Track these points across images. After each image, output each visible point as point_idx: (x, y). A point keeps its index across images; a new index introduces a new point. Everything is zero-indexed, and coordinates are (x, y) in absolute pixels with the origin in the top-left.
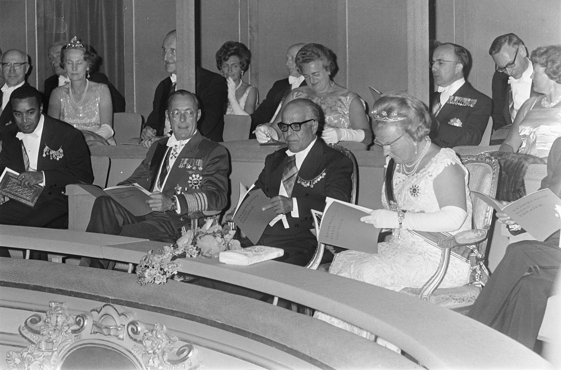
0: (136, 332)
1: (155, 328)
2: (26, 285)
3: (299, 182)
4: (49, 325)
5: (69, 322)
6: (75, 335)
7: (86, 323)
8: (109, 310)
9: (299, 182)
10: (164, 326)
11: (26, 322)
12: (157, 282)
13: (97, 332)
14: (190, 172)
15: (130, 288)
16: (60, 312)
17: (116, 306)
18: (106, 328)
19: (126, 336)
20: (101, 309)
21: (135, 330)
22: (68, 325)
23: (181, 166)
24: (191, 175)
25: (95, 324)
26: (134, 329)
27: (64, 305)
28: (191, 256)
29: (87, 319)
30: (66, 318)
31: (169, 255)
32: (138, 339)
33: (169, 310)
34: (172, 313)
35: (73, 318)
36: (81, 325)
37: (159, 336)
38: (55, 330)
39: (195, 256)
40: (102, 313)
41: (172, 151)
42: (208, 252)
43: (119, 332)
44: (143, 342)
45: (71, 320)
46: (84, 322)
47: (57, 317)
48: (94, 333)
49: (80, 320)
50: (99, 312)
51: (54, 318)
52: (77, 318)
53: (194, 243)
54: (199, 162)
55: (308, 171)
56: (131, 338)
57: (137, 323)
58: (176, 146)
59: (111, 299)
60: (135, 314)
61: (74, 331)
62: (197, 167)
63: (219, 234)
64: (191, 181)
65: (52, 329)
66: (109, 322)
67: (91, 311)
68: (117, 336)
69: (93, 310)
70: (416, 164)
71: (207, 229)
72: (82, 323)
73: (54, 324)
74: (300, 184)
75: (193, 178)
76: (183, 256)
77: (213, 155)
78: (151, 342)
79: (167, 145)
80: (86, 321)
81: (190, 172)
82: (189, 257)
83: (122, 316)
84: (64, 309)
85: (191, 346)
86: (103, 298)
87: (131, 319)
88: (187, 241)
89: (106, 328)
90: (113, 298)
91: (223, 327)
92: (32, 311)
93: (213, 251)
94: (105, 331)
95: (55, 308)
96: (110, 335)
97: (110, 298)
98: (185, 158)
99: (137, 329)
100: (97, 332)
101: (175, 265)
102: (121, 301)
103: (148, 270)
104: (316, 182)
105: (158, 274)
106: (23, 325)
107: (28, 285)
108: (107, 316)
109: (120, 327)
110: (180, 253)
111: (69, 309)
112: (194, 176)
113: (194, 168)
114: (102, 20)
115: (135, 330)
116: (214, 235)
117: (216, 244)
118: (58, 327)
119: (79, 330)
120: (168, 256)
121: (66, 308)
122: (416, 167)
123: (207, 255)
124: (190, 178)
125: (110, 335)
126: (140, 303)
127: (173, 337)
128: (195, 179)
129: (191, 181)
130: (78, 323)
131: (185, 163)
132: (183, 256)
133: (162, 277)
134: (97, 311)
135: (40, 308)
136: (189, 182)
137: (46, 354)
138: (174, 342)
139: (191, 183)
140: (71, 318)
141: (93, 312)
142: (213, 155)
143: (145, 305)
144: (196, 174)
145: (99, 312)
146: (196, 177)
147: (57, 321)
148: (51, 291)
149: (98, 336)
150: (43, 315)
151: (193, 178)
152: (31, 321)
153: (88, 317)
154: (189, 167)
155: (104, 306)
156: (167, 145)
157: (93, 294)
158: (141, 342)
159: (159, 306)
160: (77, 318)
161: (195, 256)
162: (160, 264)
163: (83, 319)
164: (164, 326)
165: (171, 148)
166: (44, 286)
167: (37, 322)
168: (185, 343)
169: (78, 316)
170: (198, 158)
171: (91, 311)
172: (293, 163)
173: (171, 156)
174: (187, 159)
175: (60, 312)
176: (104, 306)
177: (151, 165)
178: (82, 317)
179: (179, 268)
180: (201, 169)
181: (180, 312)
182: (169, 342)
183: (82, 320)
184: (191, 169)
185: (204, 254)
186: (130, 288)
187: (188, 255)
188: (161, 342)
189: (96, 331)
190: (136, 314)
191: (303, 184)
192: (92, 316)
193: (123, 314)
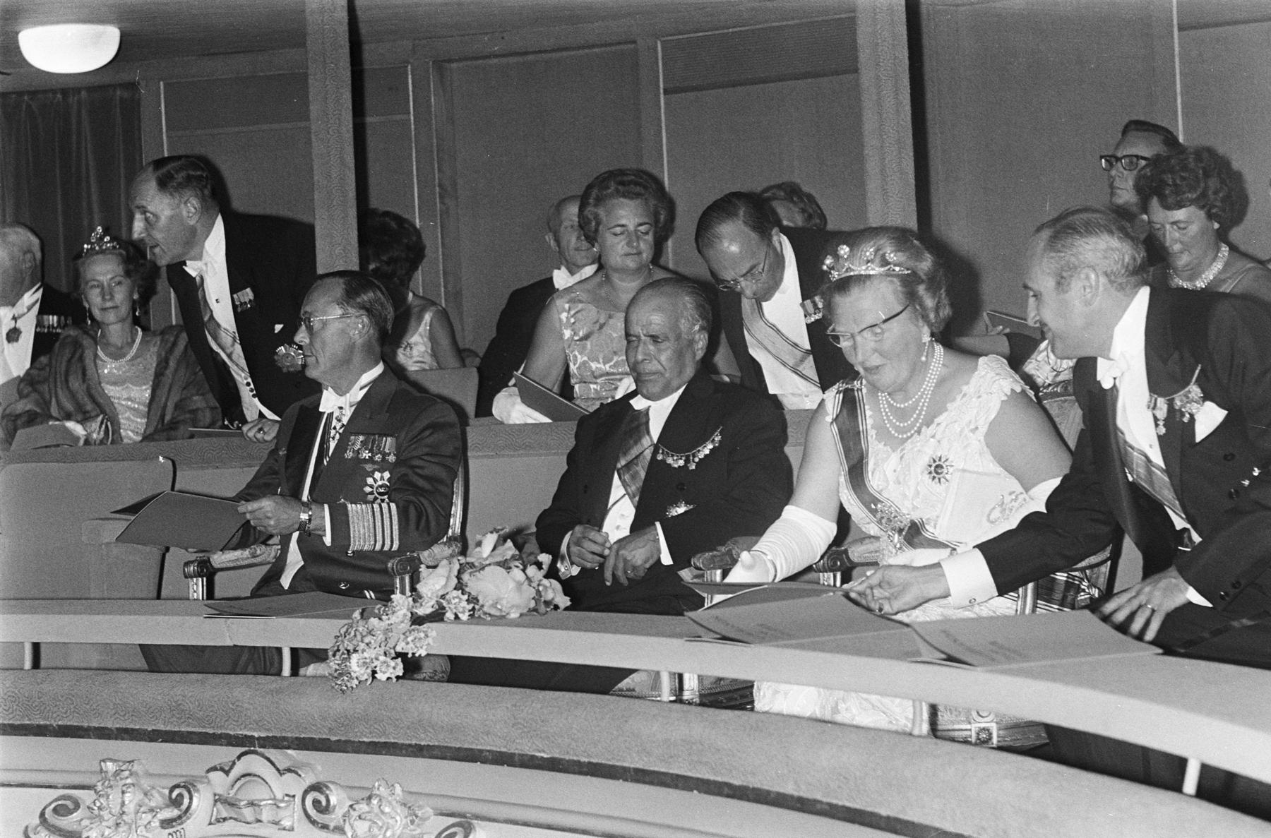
0: (323, 809)
1: (376, 792)
2: (39, 726)
3: (660, 457)
4: (105, 814)
5: (153, 804)
6: (171, 830)
7: (195, 800)
8: (254, 763)
9: (660, 457)
10: (397, 786)
11: (42, 815)
12: (381, 676)
13: (225, 819)
14: (369, 467)
15: (306, 704)
16: (129, 781)
17: (272, 753)
18: (252, 804)
19: (299, 821)
20: (234, 763)
21: (324, 803)
22: (152, 810)
23: (349, 455)
24: (371, 474)
25: (219, 799)
26: (319, 802)
27: (136, 767)
28: (457, 617)
29: (198, 791)
30: (146, 794)
31: (405, 615)
32: (332, 825)
33: (410, 745)
34: (419, 751)
35: (162, 795)
36: (184, 807)
37: (387, 810)
38: (117, 824)
39: (464, 617)
40: (235, 772)
41: (334, 423)
42: (494, 606)
43: (282, 813)
44: (347, 828)
45: (157, 800)
46: (191, 799)
47: (123, 792)
48: (218, 821)
49: (180, 795)
50: (227, 773)
51: (115, 796)
52: (171, 791)
53: (460, 586)
54: (388, 443)
55: (680, 430)
56: (313, 822)
57: (327, 787)
58: (341, 408)
59: (259, 738)
60: (319, 765)
61: (166, 823)
62: (384, 455)
63: (517, 563)
64: (371, 486)
65: (111, 823)
66: (256, 792)
67: (209, 771)
68: (276, 823)
69: (214, 769)
70: (918, 401)
71: (485, 555)
72: (186, 801)
73: (116, 810)
74: (663, 461)
75: (375, 481)
76: (437, 616)
77: (420, 425)
78: (366, 824)
79: (321, 410)
80: (196, 796)
81: (369, 467)
82: (452, 617)
83: (288, 775)
84: (136, 774)
85: (470, 824)
86: (236, 737)
87: (309, 780)
88: (443, 582)
89: (252, 804)
90: (263, 735)
91: (554, 765)
92: (56, 787)
93: (504, 602)
94: (248, 813)
95: (117, 773)
96: (259, 821)
97: (256, 735)
98: (357, 434)
99: (328, 801)
100: (225, 819)
101: (422, 635)
102: (285, 738)
103: (355, 657)
104: (701, 456)
105: (382, 658)
106: (37, 821)
107: (46, 727)
108: (248, 778)
109: (282, 801)
110: (428, 610)
111: (149, 775)
112: (377, 475)
113: (378, 458)
114: (87, 165)
115: (324, 803)
116: (505, 565)
117: (512, 585)
118: (125, 817)
119: (180, 817)
120: (401, 618)
121: (140, 773)
122: (924, 403)
123: (493, 612)
124: (370, 481)
125: (259, 821)
126: (333, 738)
127: (420, 807)
128: (380, 483)
129: (371, 486)
130: (176, 803)
131: (358, 446)
132: (437, 616)
133: (392, 663)
134: (222, 770)
135: (77, 780)
136: (368, 489)
137: (554, 592)
138: (424, 819)
139: (372, 493)
140: (157, 795)
141: (212, 775)
142: (420, 425)
143: (346, 742)
144: (382, 471)
145: (227, 773)
146: (382, 478)
147: (123, 804)
148: (103, 733)
149: (229, 827)
150: (85, 796)
151: (375, 481)
152: (55, 810)
153: (200, 786)
154: (366, 455)
155: (239, 758)
156: (321, 410)
157: (211, 731)
158: (340, 829)
159: (383, 740)
160: (171, 791)
161: (464, 617)
162: (373, 644)
163: (190, 792)
164: (397, 786)
165: (331, 415)
166: (85, 725)
167: (70, 812)
168: (452, 820)
169: (177, 786)
170: (387, 435)
171: (209, 771)
172: (643, 427)
173: (333, 432)
174: (361, 438)
175: (129, 781)
176: (239, 758)
177: (288, 457)
178: (184, 787)
179: (430, 640)
180: (392, 458)
181: (438, 747)
182: (412, 822)
183: (186, 795)
184: (371, 460)
185: (485, 609)
186: (306, 704)
187: (449, 615)
188: (391, 821)
189: (224, 814)
190: (319, 768)
191: (670, 461)
192: (209, 782)
193: (289, 770)
